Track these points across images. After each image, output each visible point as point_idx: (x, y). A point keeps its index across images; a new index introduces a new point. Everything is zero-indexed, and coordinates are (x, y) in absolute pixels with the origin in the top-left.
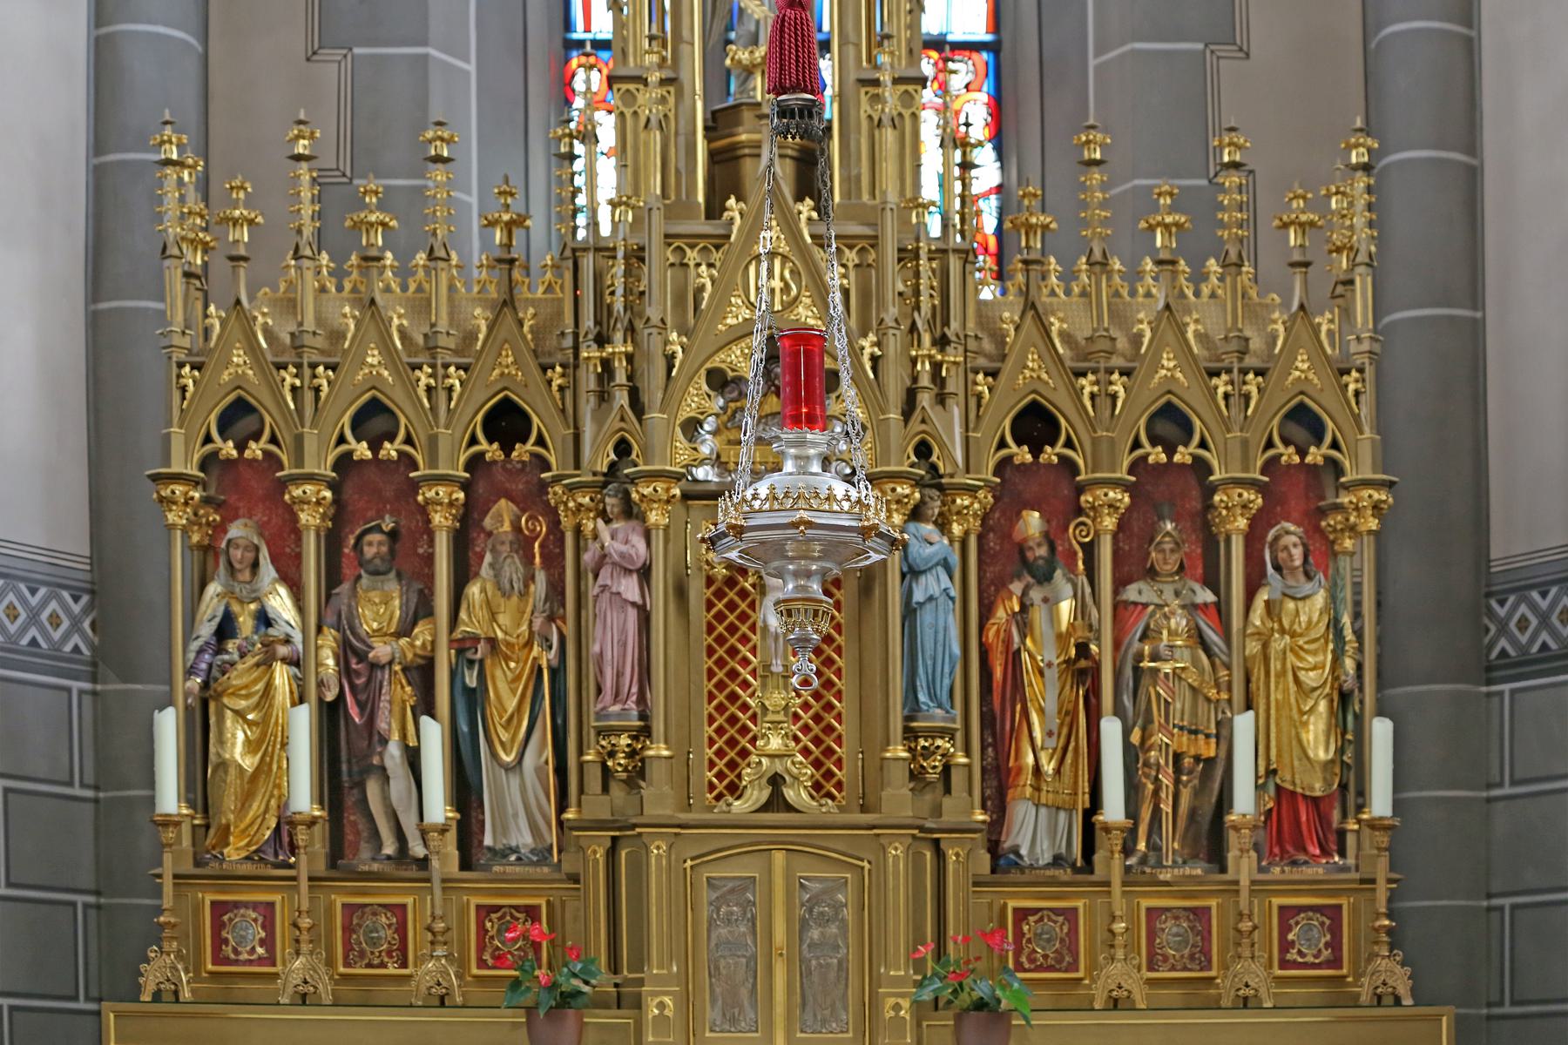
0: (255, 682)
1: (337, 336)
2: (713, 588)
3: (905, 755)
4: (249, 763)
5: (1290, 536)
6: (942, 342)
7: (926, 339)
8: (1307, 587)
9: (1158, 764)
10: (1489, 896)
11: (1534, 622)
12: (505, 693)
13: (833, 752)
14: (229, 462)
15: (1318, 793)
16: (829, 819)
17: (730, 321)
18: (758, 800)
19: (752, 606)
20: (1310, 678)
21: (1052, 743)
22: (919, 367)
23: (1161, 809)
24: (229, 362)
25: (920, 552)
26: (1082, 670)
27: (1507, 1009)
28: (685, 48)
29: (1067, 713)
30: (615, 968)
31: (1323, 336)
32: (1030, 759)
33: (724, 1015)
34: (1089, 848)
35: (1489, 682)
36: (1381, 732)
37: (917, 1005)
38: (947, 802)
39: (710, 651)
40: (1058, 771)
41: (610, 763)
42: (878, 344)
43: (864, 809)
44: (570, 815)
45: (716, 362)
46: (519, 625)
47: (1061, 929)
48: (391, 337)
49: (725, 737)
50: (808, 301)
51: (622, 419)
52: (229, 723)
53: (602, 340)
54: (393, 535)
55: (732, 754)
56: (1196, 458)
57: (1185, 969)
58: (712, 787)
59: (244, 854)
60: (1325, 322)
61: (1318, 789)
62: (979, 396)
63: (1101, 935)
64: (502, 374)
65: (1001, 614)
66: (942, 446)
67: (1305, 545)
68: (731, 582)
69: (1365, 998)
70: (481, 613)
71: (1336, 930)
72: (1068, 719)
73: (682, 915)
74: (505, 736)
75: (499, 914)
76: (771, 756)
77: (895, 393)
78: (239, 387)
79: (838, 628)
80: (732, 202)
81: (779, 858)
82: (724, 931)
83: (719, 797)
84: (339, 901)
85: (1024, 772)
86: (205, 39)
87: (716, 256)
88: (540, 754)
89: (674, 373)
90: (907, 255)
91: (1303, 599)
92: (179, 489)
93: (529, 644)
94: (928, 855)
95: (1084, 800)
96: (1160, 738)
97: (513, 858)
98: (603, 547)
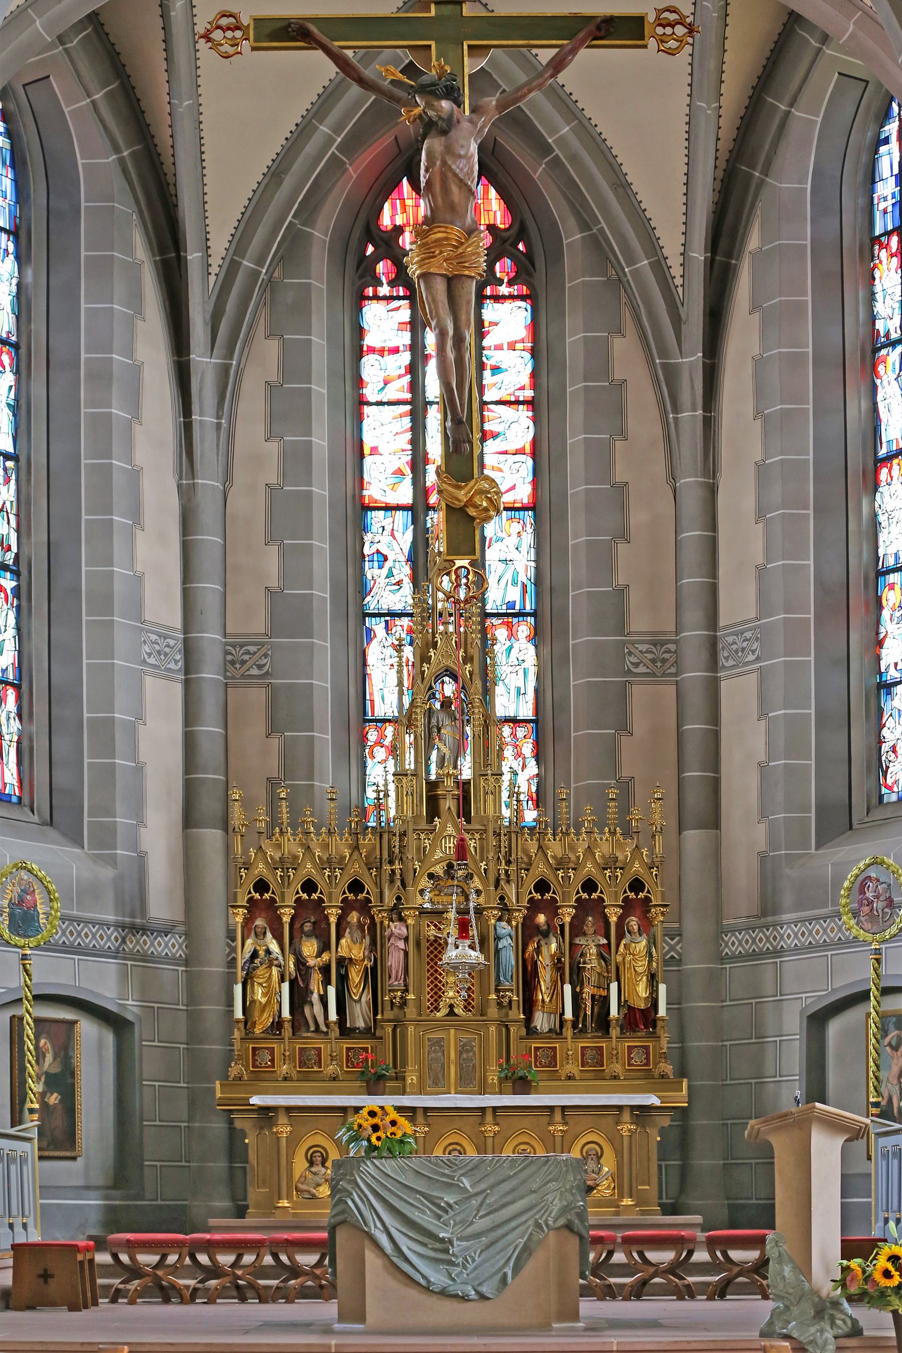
1: (295, 857)
4: (264, 1001)
5: (633, 922)
6: (508, 863)
7: (503, 862)
8: (640, 939)
10: (722, 1041)
11: (737, 943)
12: (355, 976)
14: (257, 900)
19: (443, 948)
20: (640, 970)
21: (548, 991)
24: (258, 867)
25: (501, 931)
26: (558, 966)
27: (728, 1082)
30: (395, 1066)
32: (540, 997)
34: (561, 1027)
35: (722, 964)
36: (662, 988)
37: (500, 1079)
38: (510, 1012)
39: (428, 963)
40: (550, 1001)
42: (486, 865)
43: (482, 1015)
44: (379, 1017)
45: (431, 871)
53: (391, 862)
54: (314, 923)
58: (429, 1008)
60: (645, 852)
61: (643, 1006)
62: (522, 877)
63: (565, 1055)
65: (530, 948)
66: (508, 898)
68: (435, 941)
69: (656, 1075)
70: (347, 950)
71: (648, 1054)
74: (355, 991)
77: (492, 879)
79: (473, 985)
80: (436, 819)
81: (452, 1031)
82: (433, 1055)
83: (432, 1011)
86: (226, 728)
87: (431, 836)
88: (367, 997)
92: (241, 910)
93: (363, 960)
96: (586, 990)
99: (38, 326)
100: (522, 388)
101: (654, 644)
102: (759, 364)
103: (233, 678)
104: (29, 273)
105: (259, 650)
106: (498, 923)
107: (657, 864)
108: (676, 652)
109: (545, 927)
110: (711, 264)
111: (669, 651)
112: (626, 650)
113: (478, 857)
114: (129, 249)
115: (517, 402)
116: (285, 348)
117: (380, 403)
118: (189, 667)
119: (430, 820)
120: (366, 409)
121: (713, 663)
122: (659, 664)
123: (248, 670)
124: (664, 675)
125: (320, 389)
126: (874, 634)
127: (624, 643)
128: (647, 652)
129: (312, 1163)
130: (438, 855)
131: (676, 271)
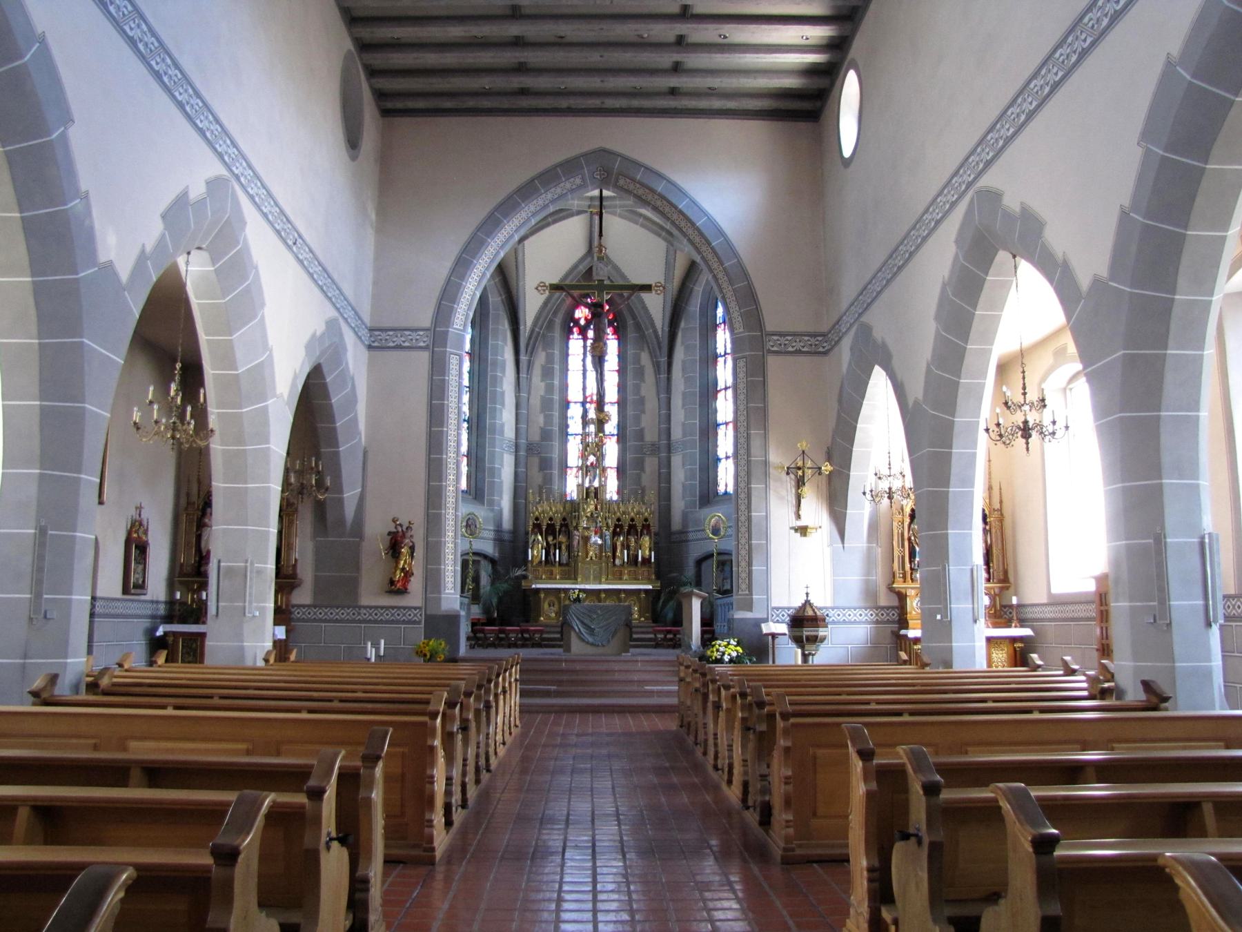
12: (563, 547)
26: (623, 545)
88: (566, 554)
99: (477, 348)
102: (684, 362)
104: (475, 333)
110: (670, 331)
114: (504, 326)
116: (547, 354)
118: (517, 451)
119: (586, 499)
125: (557, 367)
129: (550, 606)
130: (589, 510)
131: (660, 333)
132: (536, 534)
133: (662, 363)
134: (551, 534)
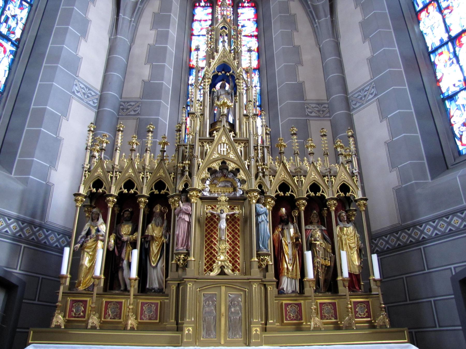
0: (93, 245)
2: (207, 221)
3: (257, 260)
9: (318, 266)
12: (155, 248)
13: (237, 262)
15: (358, 273)
16: (237, 278)
17: (213, 157)
18: (217, 272)
20: (353, 245)
21: (291, 262)
22: (259, 167)
23: (319, 278)
28: (206, 108)
29: (294, 255)
31: (347, 169)
32: (286, 266)
33: (207, 333)
40: (293, 269)
41: (178, 263)
45: (210, 166)
46: (160, 233)
47: (297, 309)
48: (135, 166)
49: (209, 258)
50: (232, 153)
51: (186, 178)
52: (85, 255)
55: (211, 262)
56: (321, 195)
57: (330, 319)
59: (84, 288)
64: (160, 175)
67: (346, 216)
72: (294, 256)
73: (196, 304)
75: (147, 305)
76: (221, 261)
77: (253, 172)
78: (98, 177)
80: (215, 132)
81: (223, 288)
82: (207, 309)
84: (104, 300)
85: (284, 270)
88: (162, 264)
89: (200, 167)
90: (256, 148)
91: (348, 227)
93: (161, 237)
94: (263, 288)
95: (299, 277)
97: (153, 291)
98: (180, 208)
100: (254, 32)
101: (318, 104)
103: (122, 115)
105: (136, 104)
106: (257, 204)
107: (356, 174)
108: (328, 107)
109: (286, 217)
111: (325, 107)
112: (306, 107)
113: (243, 158)
115: (251, 36)
117: (199, 36)
120: (193, 37)
121: (348, 107)
122: (321, 112)
123: (130, 112)
124: (324, 117)
126: (434, 78)
127: (304, 104)
128: (315, 107)
130: (216, 156)
132: (95, 219)
133: (321, 8)
134: (128, 220)
